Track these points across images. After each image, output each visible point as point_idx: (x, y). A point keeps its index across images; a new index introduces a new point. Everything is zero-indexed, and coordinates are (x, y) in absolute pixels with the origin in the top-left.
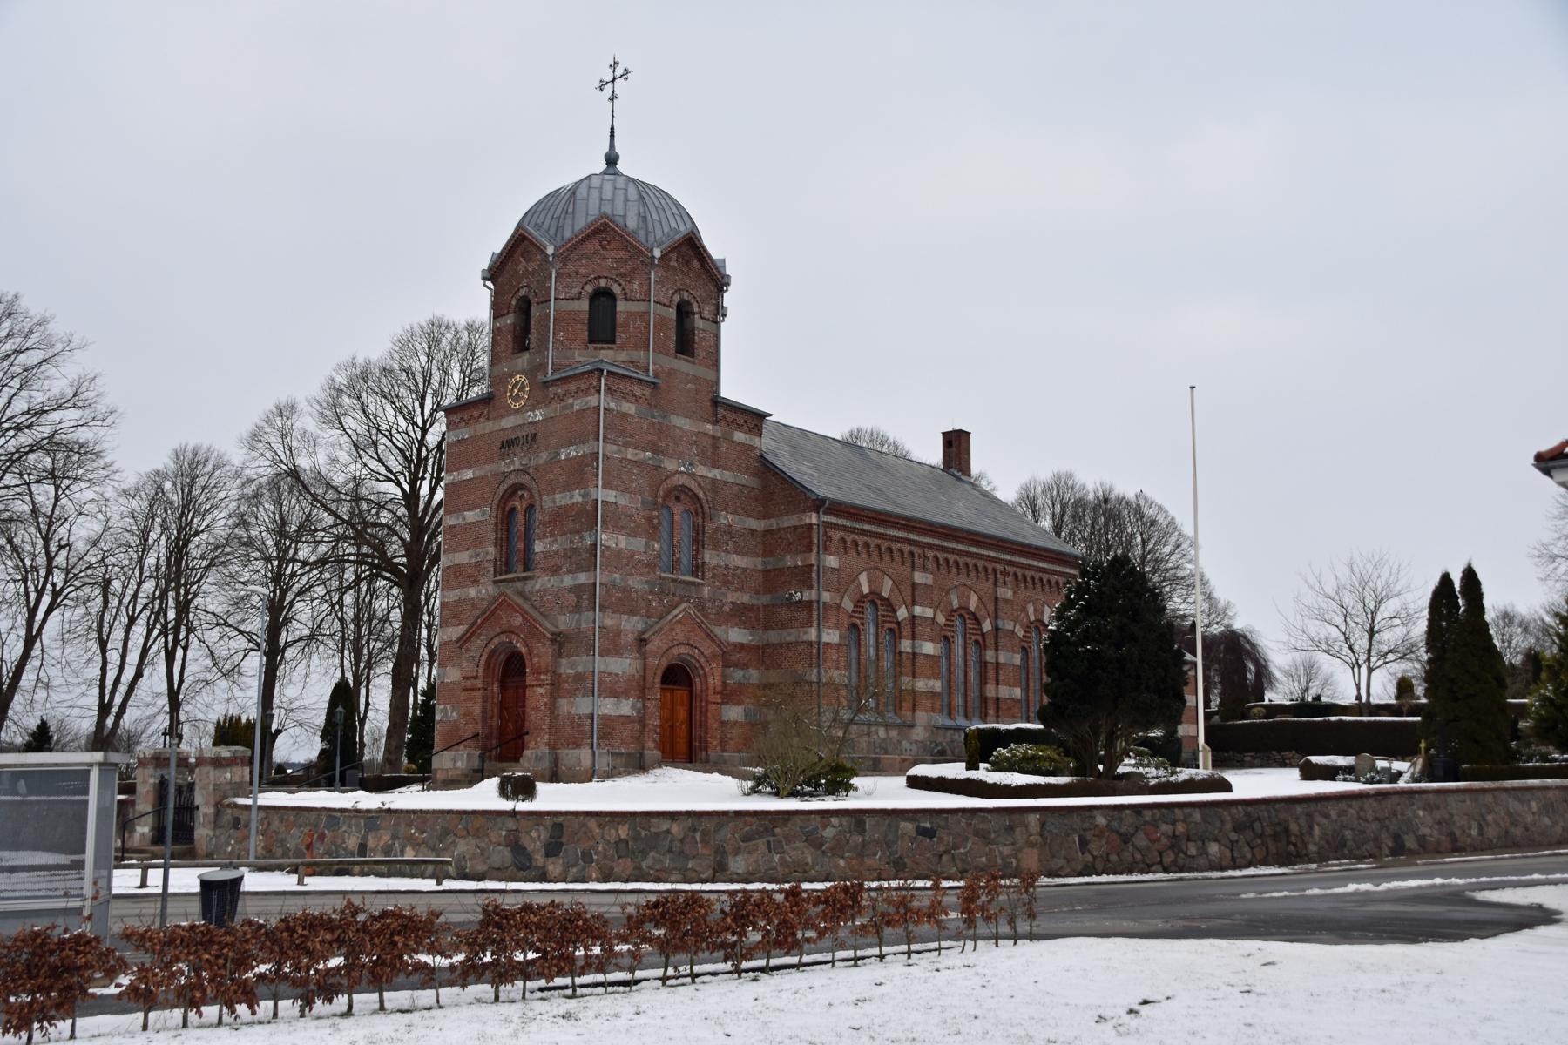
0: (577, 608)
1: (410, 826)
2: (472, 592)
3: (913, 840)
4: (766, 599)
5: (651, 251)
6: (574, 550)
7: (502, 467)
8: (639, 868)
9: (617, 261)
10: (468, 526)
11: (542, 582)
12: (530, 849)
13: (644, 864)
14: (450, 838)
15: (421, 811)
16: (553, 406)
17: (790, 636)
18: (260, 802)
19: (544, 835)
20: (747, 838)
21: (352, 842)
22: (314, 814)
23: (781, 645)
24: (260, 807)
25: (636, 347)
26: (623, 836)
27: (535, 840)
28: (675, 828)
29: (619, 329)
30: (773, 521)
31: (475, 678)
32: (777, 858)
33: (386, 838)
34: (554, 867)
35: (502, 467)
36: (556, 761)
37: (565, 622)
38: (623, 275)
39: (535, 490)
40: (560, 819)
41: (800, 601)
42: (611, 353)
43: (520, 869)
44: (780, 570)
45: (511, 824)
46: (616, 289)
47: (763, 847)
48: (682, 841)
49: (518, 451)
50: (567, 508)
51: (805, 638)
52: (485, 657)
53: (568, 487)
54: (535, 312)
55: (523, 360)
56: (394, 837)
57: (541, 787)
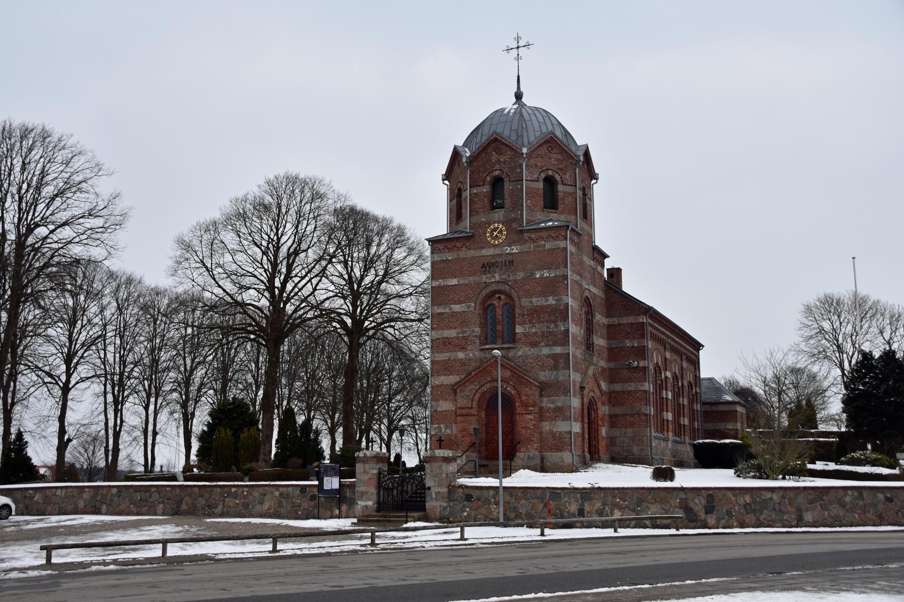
0: (555, 367)
1: (614, 497)
2: (461, 355)
3: (884, 503)
4: (612, 365)
5: (521, 150)
6: (551, 333)
7: (484, 278)
8: (758, 519)
9: (557, 160)
10: (454, 314)
11: (522, 351)
12: (696, 509)
13: (761, 517)
14: (645, 505)
15: (623, 488)
16: (528, 245)
17: (631, 387)
18: (504, 485)
19: (704, 502)
20: (811, 502)
21: (574, 508)
22: (539, 492)
23: (623, 392)
24: (505, 488)
25: (569, 213)
26: (748, 501)
27: (698, 505)
28: (775, 497)
29: (560, 202)
30: (615, 319)
31: (471, 408)
32: (826, 513)
33: (598, 505)
34: (711, 520)
35: (484, 278)
36: (542, 459)
37: (545, 375)
38: (561, 169)
39: (514, 295)
40: (711, 492)
41: (637, 367)
42: (556, 215)
43: (690, 521)
44: (623, 349)
45: (682, 495)
46: (558, 177)
47: (819, 508)
48: (779, 504)
49: (498, 270)
50: (542, 307)
51: (642, 388)
52: (478, 395)
53: (544, 294)
54: (508, 186)
55: (499, 214)
56: (604, 504)
57: (678, 472)
